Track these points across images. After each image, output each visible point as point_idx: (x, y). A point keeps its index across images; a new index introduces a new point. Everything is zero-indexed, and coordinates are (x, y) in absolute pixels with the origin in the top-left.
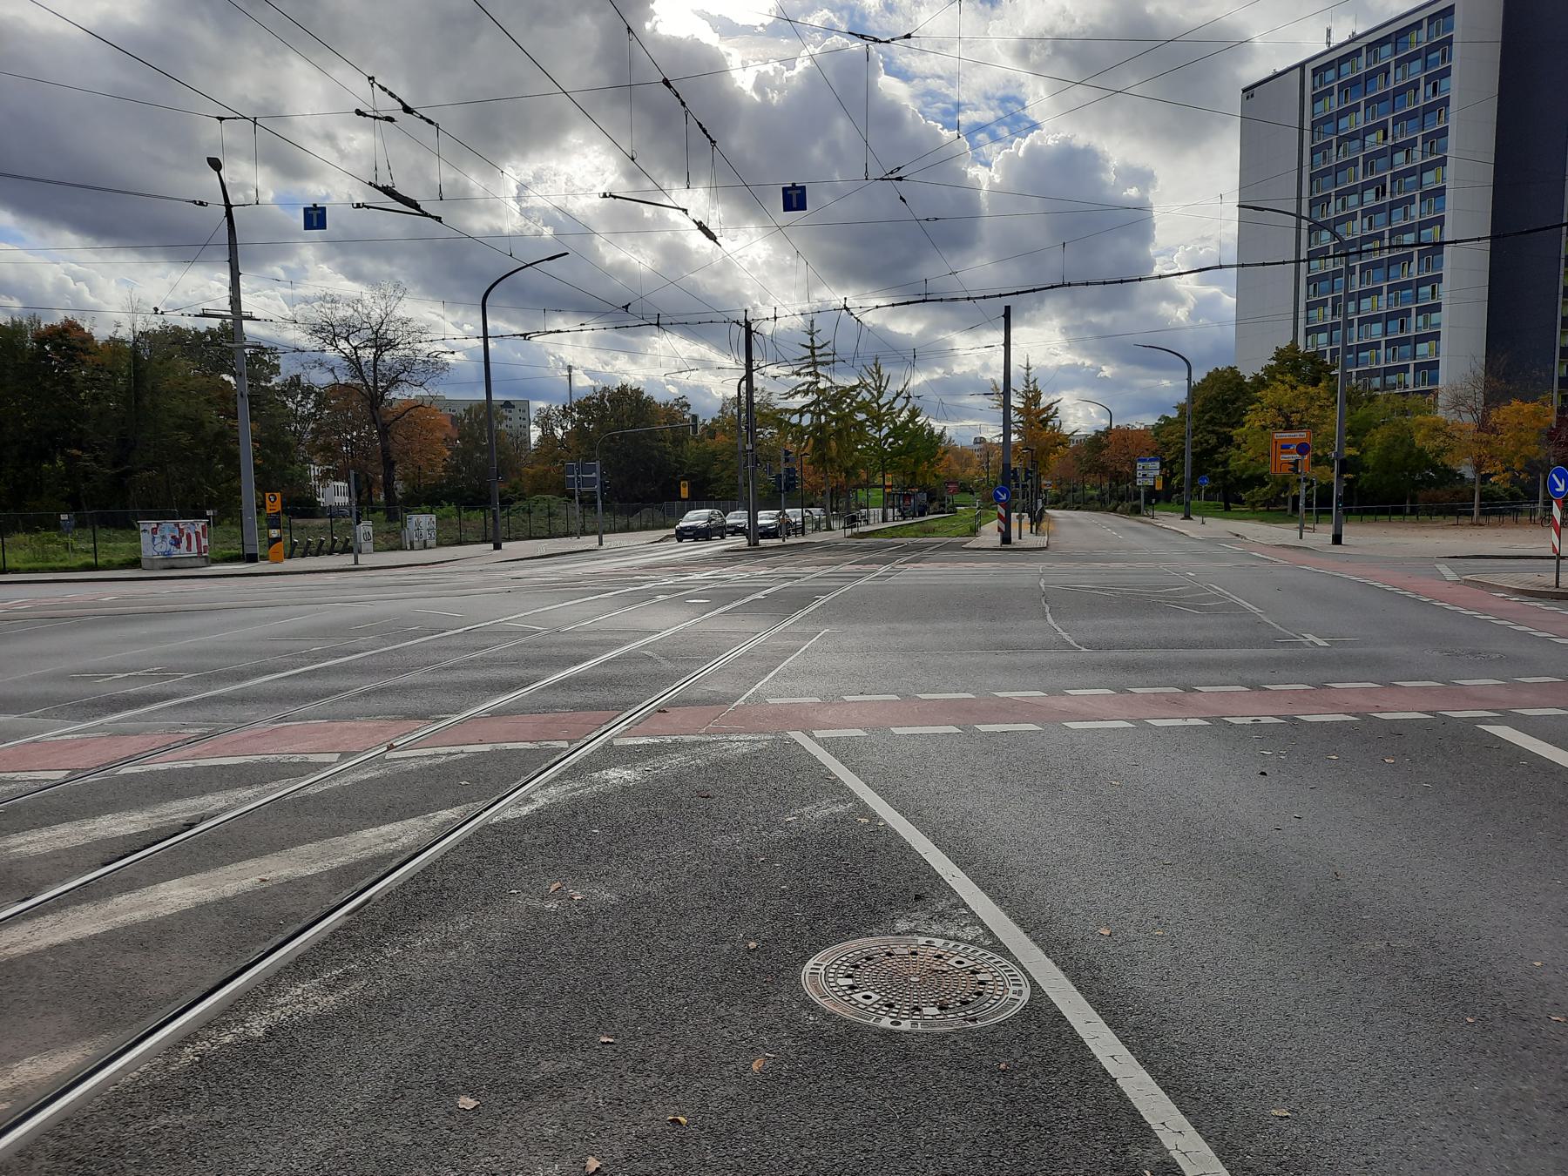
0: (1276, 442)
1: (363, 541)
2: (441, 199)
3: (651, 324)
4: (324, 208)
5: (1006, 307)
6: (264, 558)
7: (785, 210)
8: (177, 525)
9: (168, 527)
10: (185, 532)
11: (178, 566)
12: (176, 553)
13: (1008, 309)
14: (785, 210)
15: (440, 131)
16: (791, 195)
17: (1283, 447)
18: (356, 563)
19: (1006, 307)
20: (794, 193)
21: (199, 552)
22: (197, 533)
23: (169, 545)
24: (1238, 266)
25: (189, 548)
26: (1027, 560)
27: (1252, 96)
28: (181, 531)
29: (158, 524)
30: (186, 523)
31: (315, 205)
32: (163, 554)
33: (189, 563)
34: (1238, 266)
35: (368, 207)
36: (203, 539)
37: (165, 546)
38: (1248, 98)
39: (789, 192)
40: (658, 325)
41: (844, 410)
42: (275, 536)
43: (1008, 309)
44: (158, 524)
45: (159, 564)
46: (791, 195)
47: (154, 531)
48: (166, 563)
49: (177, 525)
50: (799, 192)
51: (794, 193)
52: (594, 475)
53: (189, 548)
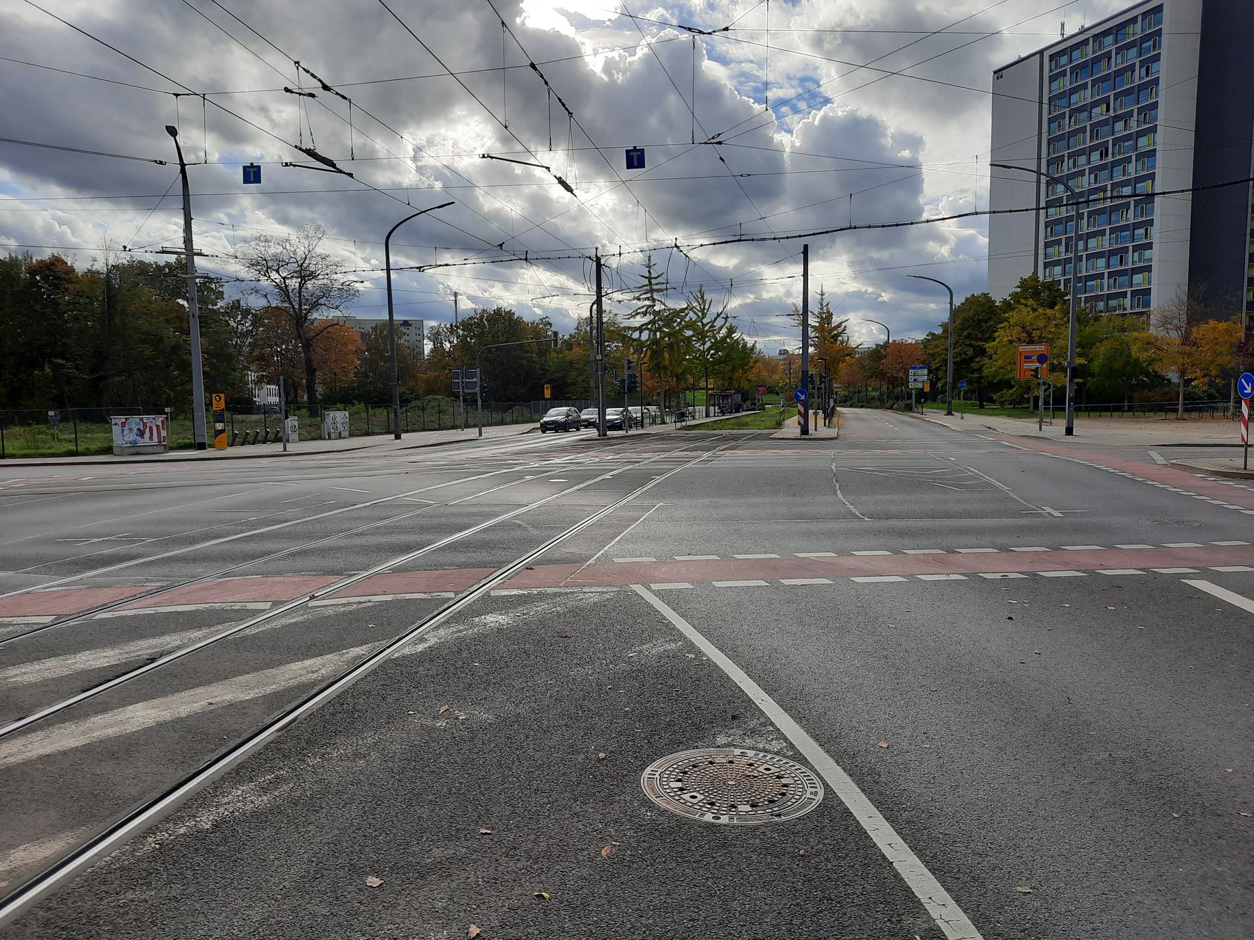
0: (1021, 354)
1: (290, 432)
2: (353, 159)
3: (520, 259)
4: (260, 166)
5: (804, 245)
6: (211, 446)
7: (628, 168)
8: (142, 419)
9: (134, 421)
10: (148, 425)
11: (142, 452)
12: (141, 442)
13: (806, 247)
14: (628, 168)
16: (633, 156)
17: (1026, 357)
19: (804, 245)
20: (635, 154)
21: (159, 442)
22: (157, 426)
23: (135, 436)
25: (151, 438)
27: (1002, 76)
28: (145, 424)
29: (126, 419)
30: (149, 418)
31: (252, 164)
32: (131, 443)
33: (151, 450)
35: (295, 166)
36: (162, 431)
37: (132, 437)
38: (998, 78)
39: (631, 154)
40: (526, 259)
42: (220, 428)
43: (806, 247)
44: (126, 419)
45: (127, 451)
46: (633, 156)
47: (123, 425)
48: (133, 450)
49: (142, 419)
50: (639, 153)
51: (635, 154)
53: (151, 438)
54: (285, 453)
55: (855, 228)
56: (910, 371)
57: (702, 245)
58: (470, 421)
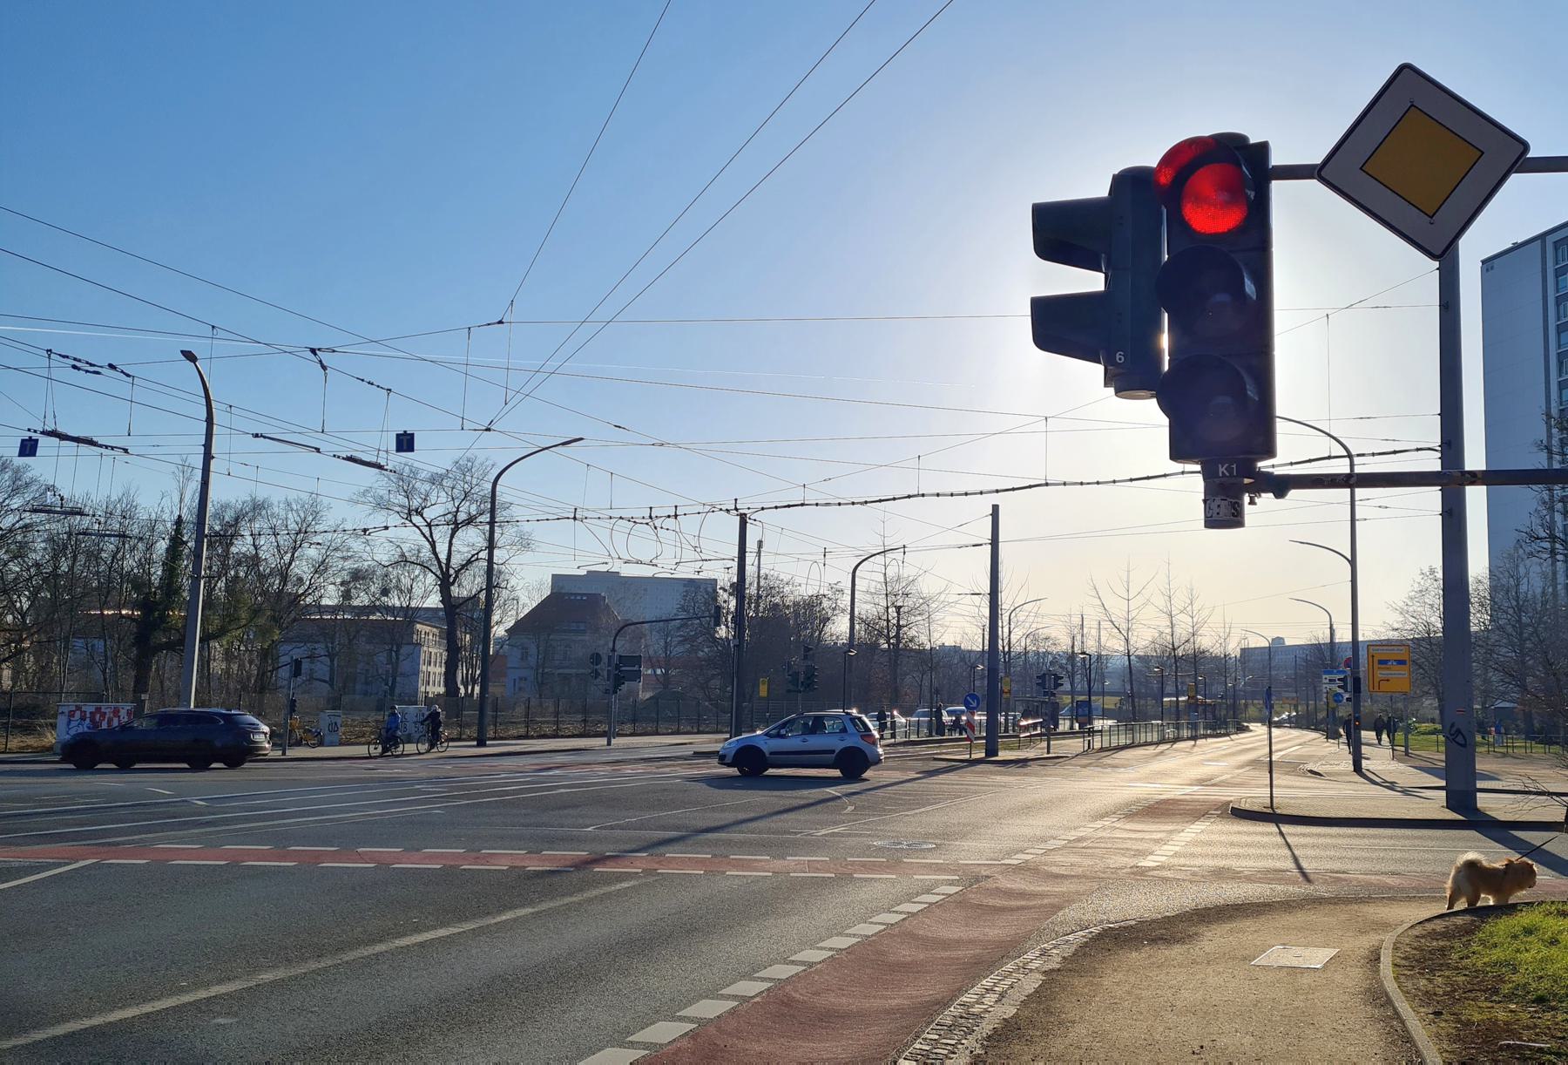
0: (1373, 656)
2: (129, 435)
3: (568, 518)
4: (413, 434)
5: (993, 505)
7: (553, 575)
13: (995, 508)
14: (553, 575)
15: (1346, 454)
16: (402, 440)
17: (1381, 662)
18: (284, 754)
19: (993, 505)
20: (405, 438)
24: (1271, 761)
26: (1000, 773)
31: (405, 432)
34: (1271, 761)
35: (265, 437)
39: (25, 443)
40: (575, 518)
41: (470, 696)
43: (995, 508)
46: (402, 440)
50: (33, 443)
51: (405, 438)
52: (192, 706)
54: (608, 747)
55: (923, 495)
56: (985, 735)
57: (763, 509)
58: (659, 730)
